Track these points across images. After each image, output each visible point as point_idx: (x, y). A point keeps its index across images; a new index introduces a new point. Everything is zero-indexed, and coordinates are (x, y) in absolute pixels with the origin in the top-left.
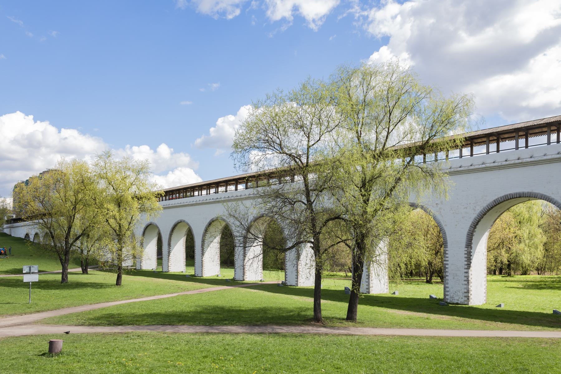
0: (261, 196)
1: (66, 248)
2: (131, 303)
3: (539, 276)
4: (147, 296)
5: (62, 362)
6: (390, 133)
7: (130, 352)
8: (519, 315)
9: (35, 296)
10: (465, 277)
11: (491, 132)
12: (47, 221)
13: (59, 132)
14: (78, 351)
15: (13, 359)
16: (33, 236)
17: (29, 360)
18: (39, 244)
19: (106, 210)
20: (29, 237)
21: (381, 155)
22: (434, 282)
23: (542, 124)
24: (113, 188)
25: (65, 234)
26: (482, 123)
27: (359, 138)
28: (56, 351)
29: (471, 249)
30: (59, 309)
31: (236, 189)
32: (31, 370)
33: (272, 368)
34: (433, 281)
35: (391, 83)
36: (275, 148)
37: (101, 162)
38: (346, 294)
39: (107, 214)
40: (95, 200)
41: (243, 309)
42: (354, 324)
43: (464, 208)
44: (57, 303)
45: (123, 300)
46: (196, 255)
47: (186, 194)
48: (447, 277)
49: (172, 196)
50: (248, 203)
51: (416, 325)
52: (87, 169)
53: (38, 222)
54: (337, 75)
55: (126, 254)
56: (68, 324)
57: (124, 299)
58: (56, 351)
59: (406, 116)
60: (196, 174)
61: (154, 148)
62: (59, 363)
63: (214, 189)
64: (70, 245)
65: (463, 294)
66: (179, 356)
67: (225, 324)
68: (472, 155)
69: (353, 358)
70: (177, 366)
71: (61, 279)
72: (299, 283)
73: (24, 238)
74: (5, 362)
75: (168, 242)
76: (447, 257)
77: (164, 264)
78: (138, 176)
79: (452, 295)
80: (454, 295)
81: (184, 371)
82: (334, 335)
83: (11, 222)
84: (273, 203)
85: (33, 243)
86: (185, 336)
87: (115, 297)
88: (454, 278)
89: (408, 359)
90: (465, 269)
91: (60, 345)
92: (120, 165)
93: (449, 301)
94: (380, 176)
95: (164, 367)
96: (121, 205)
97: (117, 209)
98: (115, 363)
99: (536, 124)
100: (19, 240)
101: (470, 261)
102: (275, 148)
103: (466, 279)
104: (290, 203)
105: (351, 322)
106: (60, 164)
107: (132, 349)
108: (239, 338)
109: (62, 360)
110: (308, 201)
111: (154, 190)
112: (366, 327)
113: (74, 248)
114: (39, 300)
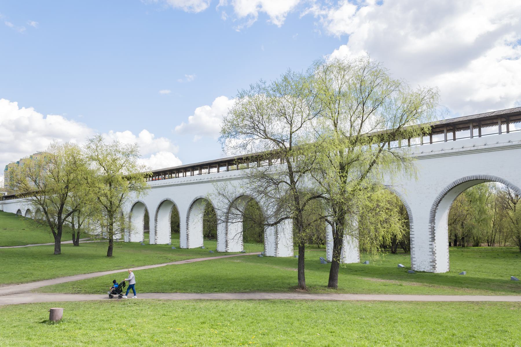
0: (248, 177)
1: (59, 222)
2: (123, 272)
3: (489, 247)
4: (138, 266)
5: (64, 330)
6: (364, 121)
7: (129, 318)
8: (481, 282)
9: (29, 267)
10: (430, 248)
11: (448, 122)
12: (41, 198)
13: (45, 117)
14: (78, 318)
15: (15, 327)
16: (25, 212)
17: (30, 327)
18: (31, 219)
19: (98, 189)
20: (21, 213)
21: (355, 141)
22: (399, 253)
23: (493, 116)
24: (105, 169)
25: (58, 210)
26: (446, 113)
27: (335, 125)
28: (57, 319)
29: (435, 224)
30: (54, 278)
31: (218, 172)
32: (34, 337)
33: (269, 333)
34: (397, 252)
35: (363, 77)
36: (260, 133)
37: (93, 146)
38: (321, 263)
39: (99, 192)
40: (87, 179)
41: (230, 277)
42: (335, 290)
43: (427, 189)
44: (52, 273)
45: (115, 270)
46: (181, 229)
47: (171, 176)
48: (413, 249)
49: (158, 177)
50: (236, 183)
51: (392, 292)
52: (79, 151)
53: (31, 199)
54: (314, 69)
55: (117, 228)
56: (65, 293)
57: (116, 268)
58: (57, 319)
59: (378, 107)
60: (176, 157)
61: (136, 134)
62: (61, 330)
63: (190, 172)
64: (62, 220)
65: (428, 263)
66: (177, 322)
67: (216, 291)
68: (431, 143)
69: (344, 323)
70: (177, 332)
71: (54, 251)
72: (277, 254)
73: (16, 213)
74: (7, 330)
75: (155, 217)
76: (413, 231)
77: (150, 237)
78: (128, 159)
79: (418, 264)
80: (421, 264)
81: (185, 337)
82: (320, 301)
83: (3, 198)
84: (259, 183)
85: (25, 218)
86: (180, 303)
87: (107, 267)
88: (420, 250)
89: (394, 322)
90: (430, 241)
91: (61, 312)
92: (111, 148)
93: (416, 270)
94: (357, 159)
95: (165, 333)
96: (112, 184)
97: (108, 187)
98: (116, 330)
99: (488, 116)
100: (11, 215)
101: (434, 235)
102: (260, 133)
103: (431, 250)
104: (275, 183)
105: (332, 289)
106: (53, 146)
107: (130, 316)
108: (231, 305)
109: (63, 327)
110: (292, 181)
111: (143, 171)
112: (346, 293)
113: (67, 223)
114: (34, 270)
